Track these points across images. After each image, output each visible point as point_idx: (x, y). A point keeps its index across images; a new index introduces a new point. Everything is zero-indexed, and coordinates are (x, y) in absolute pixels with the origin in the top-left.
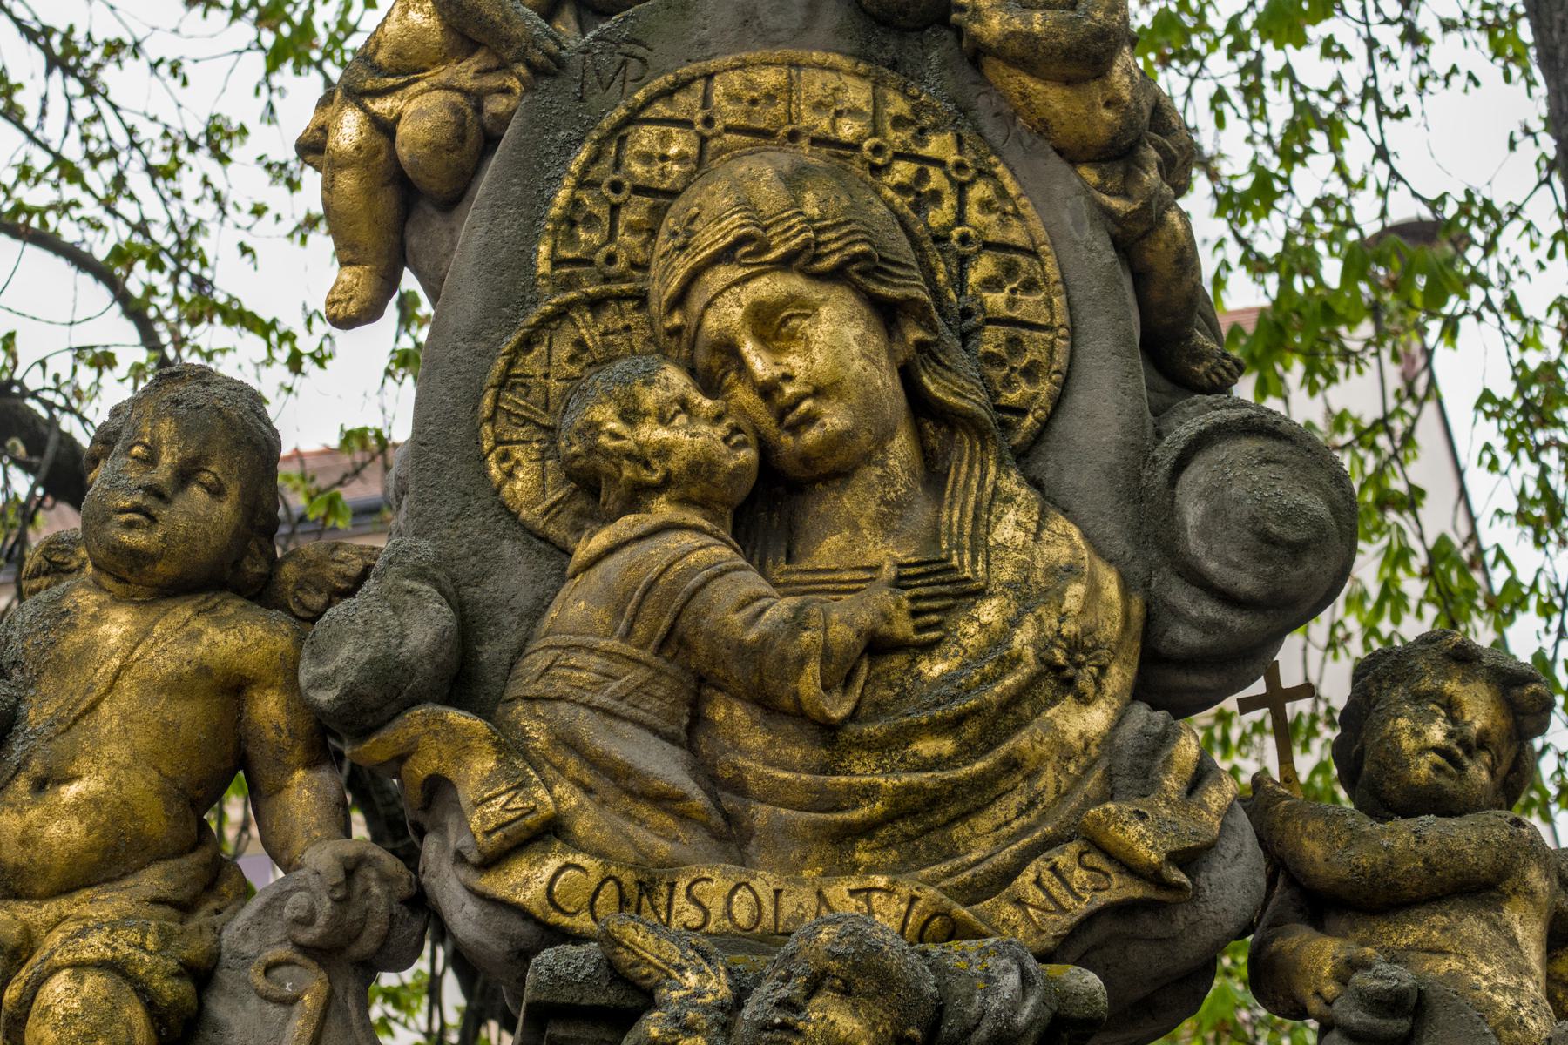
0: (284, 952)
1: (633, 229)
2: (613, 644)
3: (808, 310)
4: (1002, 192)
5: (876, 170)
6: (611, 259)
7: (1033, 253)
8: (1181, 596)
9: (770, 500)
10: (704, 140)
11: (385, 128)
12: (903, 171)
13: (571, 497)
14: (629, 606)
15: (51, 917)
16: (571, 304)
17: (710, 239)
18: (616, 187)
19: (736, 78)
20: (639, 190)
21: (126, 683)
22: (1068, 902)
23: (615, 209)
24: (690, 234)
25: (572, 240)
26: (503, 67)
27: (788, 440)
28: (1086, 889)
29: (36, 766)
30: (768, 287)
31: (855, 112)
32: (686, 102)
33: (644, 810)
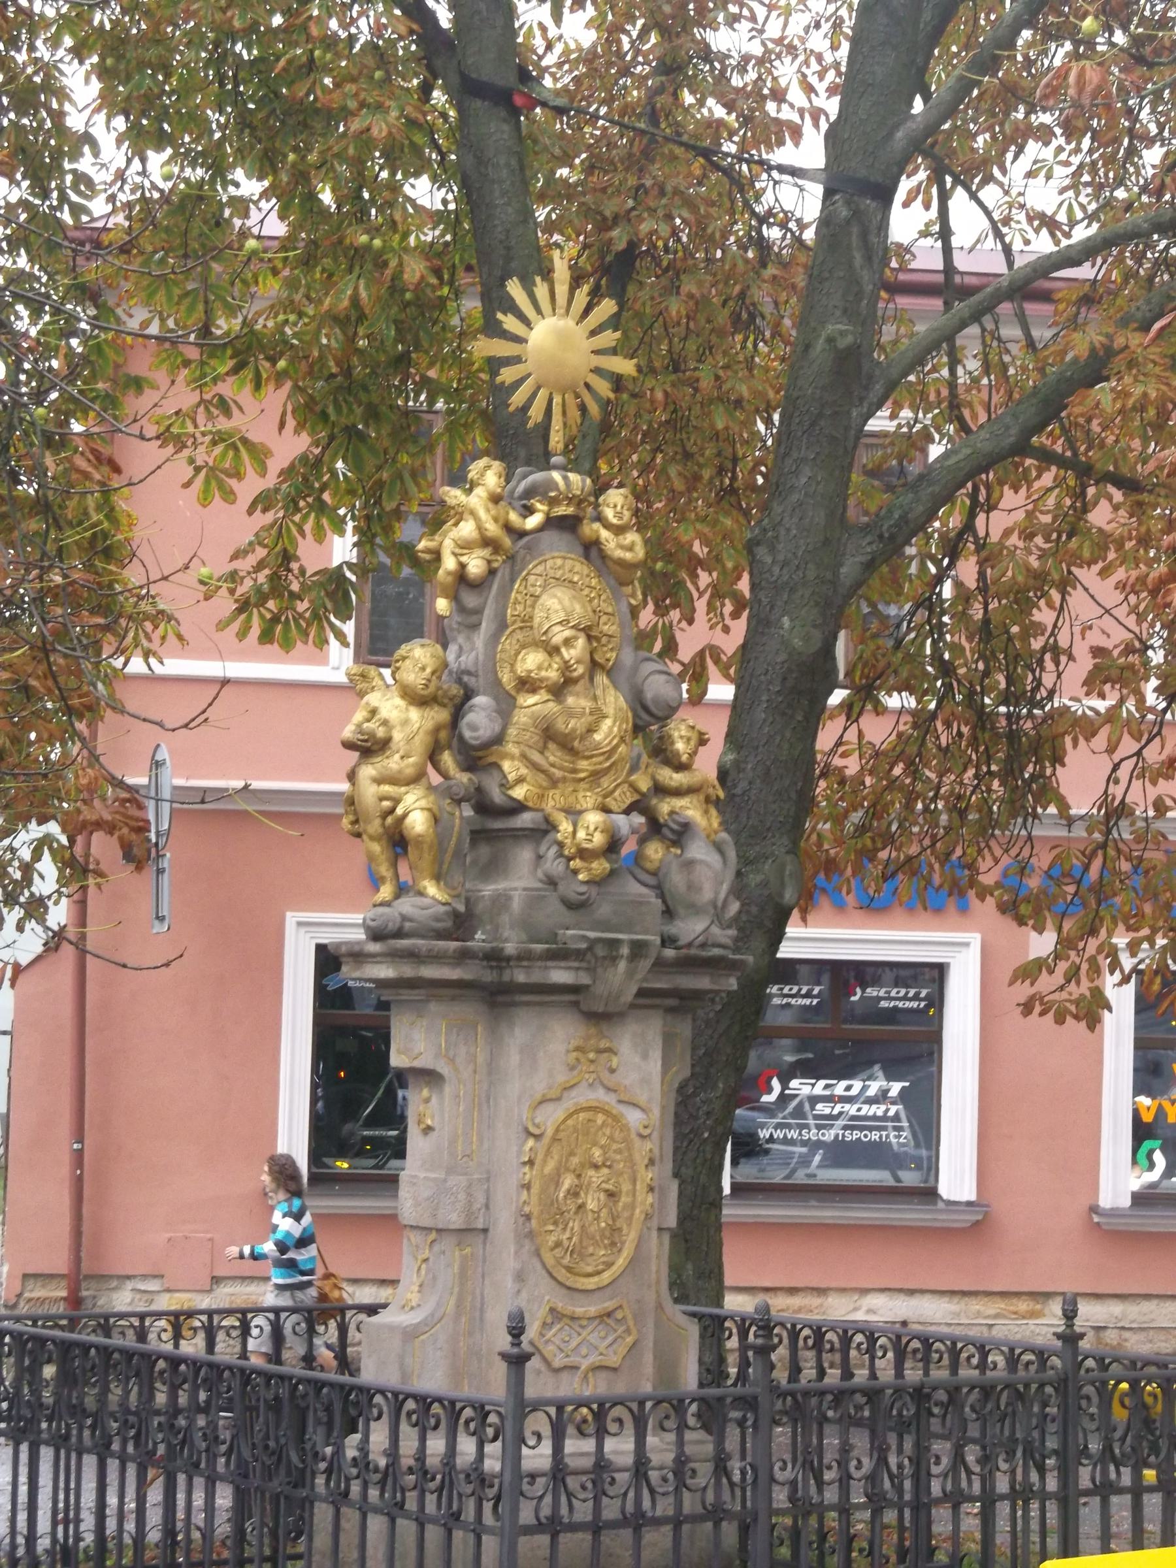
3: (576, 638)
30: (568, 633)
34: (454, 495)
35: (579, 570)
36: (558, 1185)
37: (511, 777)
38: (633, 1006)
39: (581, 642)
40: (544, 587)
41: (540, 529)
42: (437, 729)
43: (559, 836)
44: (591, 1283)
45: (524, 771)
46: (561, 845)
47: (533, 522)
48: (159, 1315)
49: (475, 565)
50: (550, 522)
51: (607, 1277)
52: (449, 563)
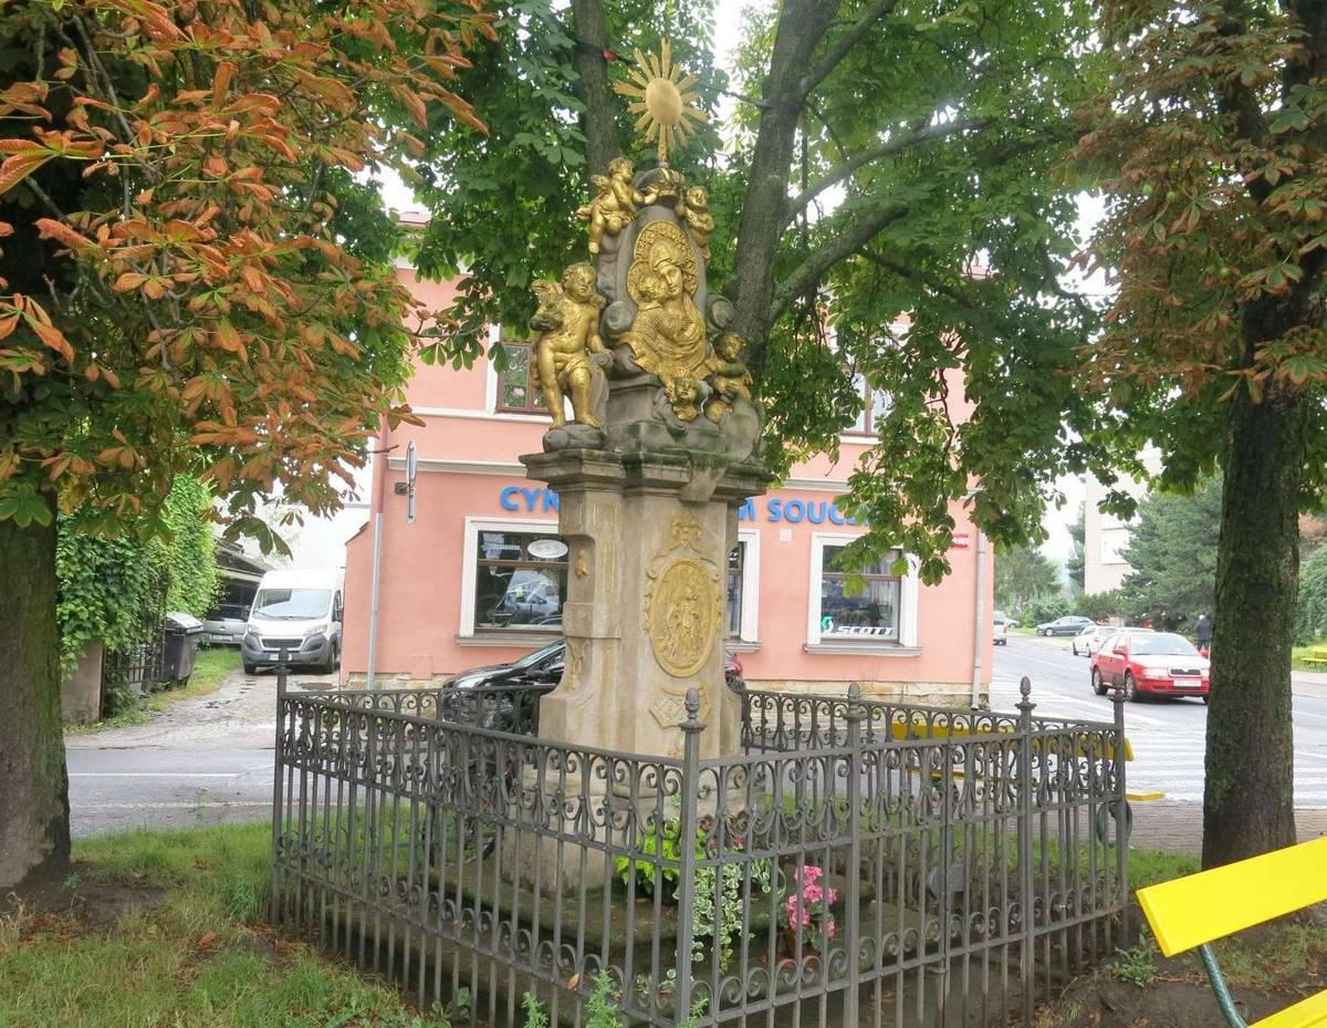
34: (601, 180)
35: (675, 232)
36: (666, 611)
38: (712, 500)
39: (678, 274)
41: (652, 204)
42: (591, 320)
44: (684, 673)
46: (668, 395)
47: (648, 199)
48: (409, 692)
49: (615, 220)
51: (694, 669)
52: (599, 219)
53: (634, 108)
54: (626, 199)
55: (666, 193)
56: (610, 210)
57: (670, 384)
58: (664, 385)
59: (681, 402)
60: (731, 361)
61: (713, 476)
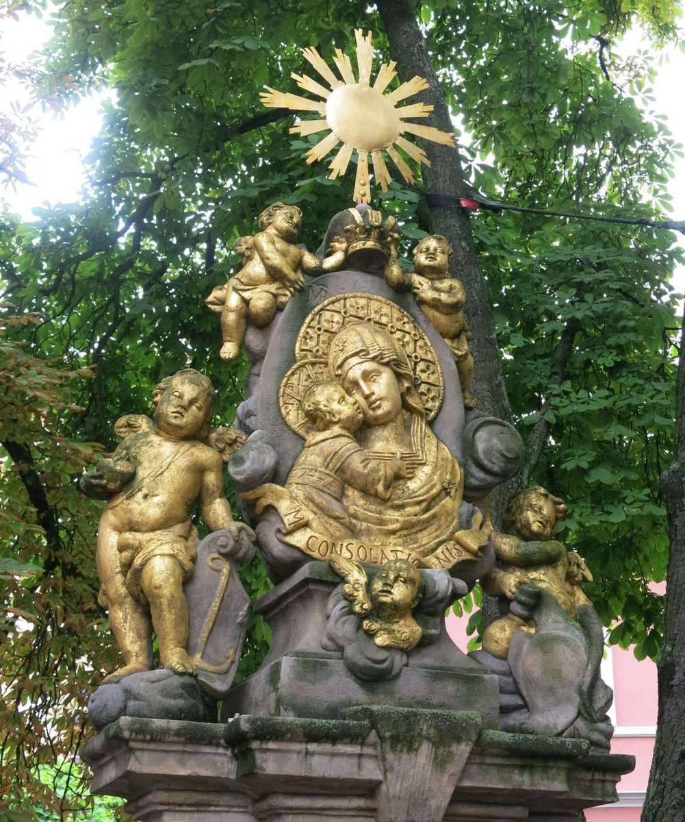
0: (216, 555)
1: (324, 342)
2: (323, 469)
3: (378, 373)
4: (426, 344)
5: (392, 333)
6: (317, 351)
7: (434, 363)
8: (474, 470)
9: (361, 429)
10: (344, 318)
11: (246, 302)
12: (398, 335)
13: (307, 422)
14: (328, 459)
15: (148, 538)
16: (306, 363)
17: (351, 349)
18: (319, 329)
19: (353, 300)
20: (326, 331)
21: (172, 466)
22: (451, 559)
23: (319, 335)
24: (344, 347)
25: (306, 344)
26: (285, 287)
27: (371, 412)
28: (456, 557)
29: (145, 491)
30: (369, 366)
31: (386, 315)
32: (338, 306)
33: (331, 521)
35: (387, 311)
37: (289, 520)
39: (386, 377)
40: (343, 325)
43: (347, 588)
45: (307, 514)
47: (329, 263)
50: (351, 262)
53: (302, 127)
54: (276, 260)
55: (359, 245)
56: (253, 283)
57: (357, 577)
58: (343, 579)
59: (381, 611)
60: (526, 535)
61: (440, 763)
